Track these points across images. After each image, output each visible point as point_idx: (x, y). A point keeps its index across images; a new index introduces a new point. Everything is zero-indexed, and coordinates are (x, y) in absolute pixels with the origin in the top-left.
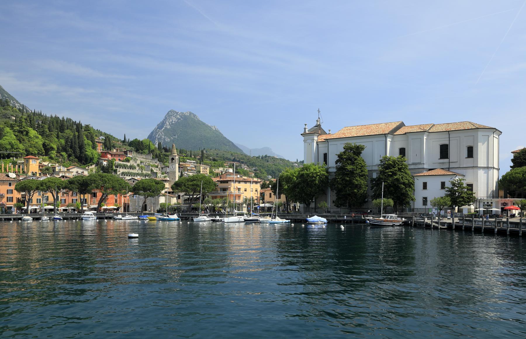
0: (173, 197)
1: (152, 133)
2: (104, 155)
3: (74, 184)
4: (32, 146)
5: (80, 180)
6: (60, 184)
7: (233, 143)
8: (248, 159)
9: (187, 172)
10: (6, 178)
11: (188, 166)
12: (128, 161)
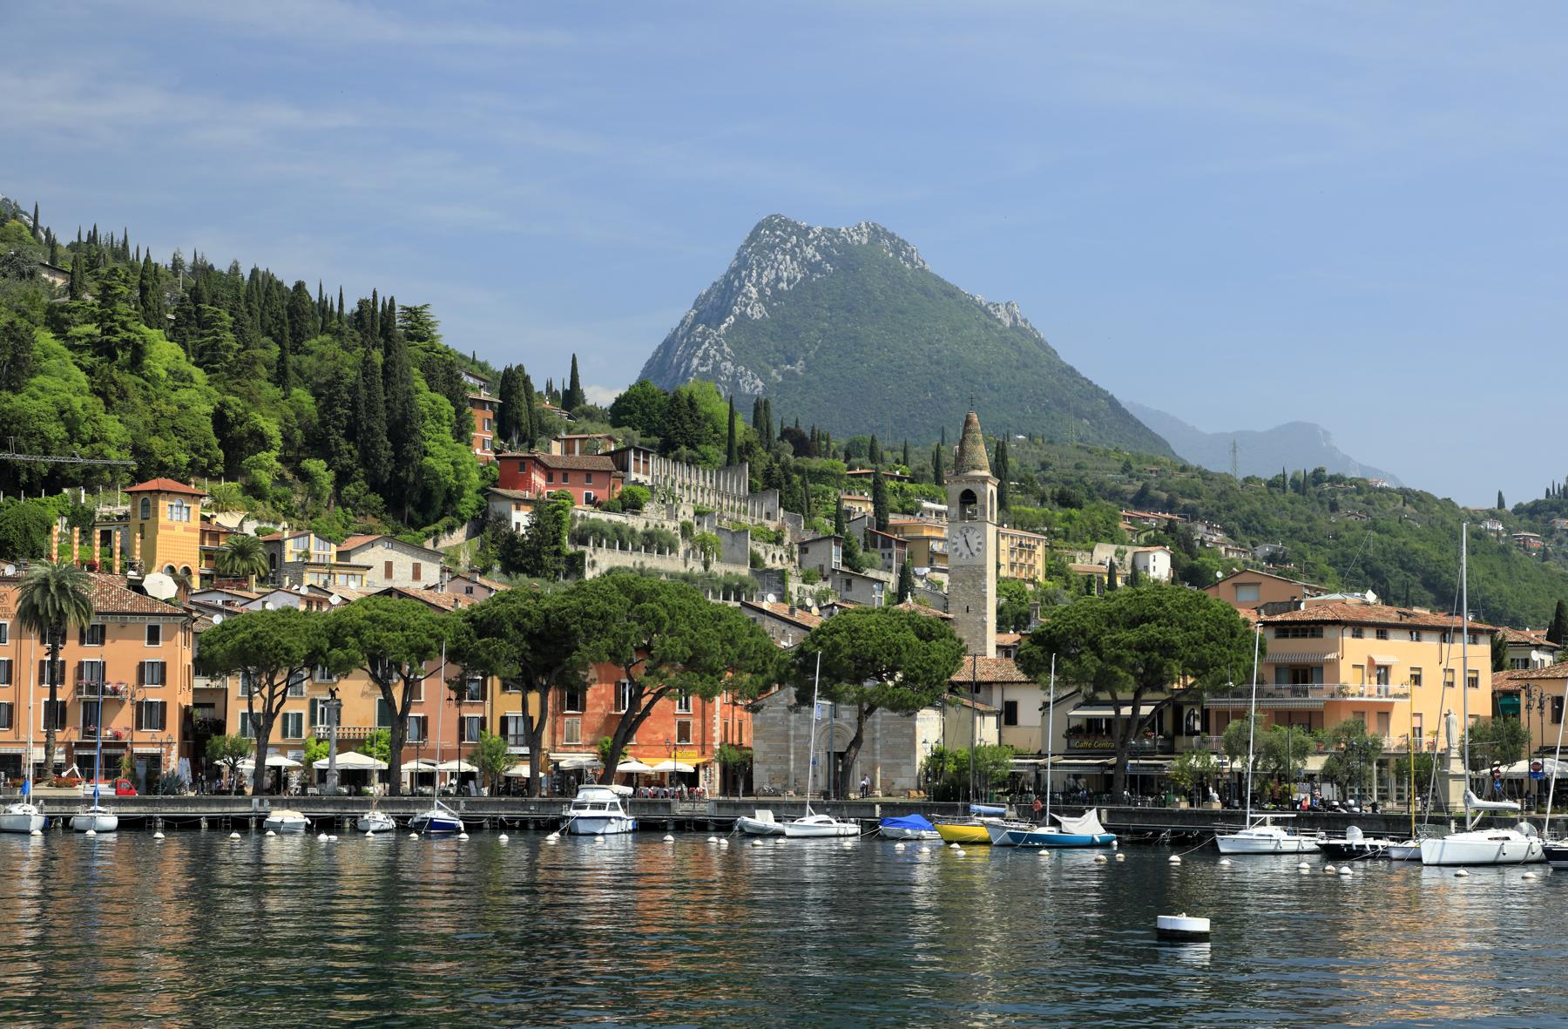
0: (982, 714)
1: (667, 346)
2: (511, 472)
3: (501, 635)
4: (163, 424)
5: (527, 615)
6: (431, 636)
7: (1112, 402)
8: (1222, 495)
9: (927, 570)
10: (131, 601)
11: (934, 534)
12: (632, 505)
